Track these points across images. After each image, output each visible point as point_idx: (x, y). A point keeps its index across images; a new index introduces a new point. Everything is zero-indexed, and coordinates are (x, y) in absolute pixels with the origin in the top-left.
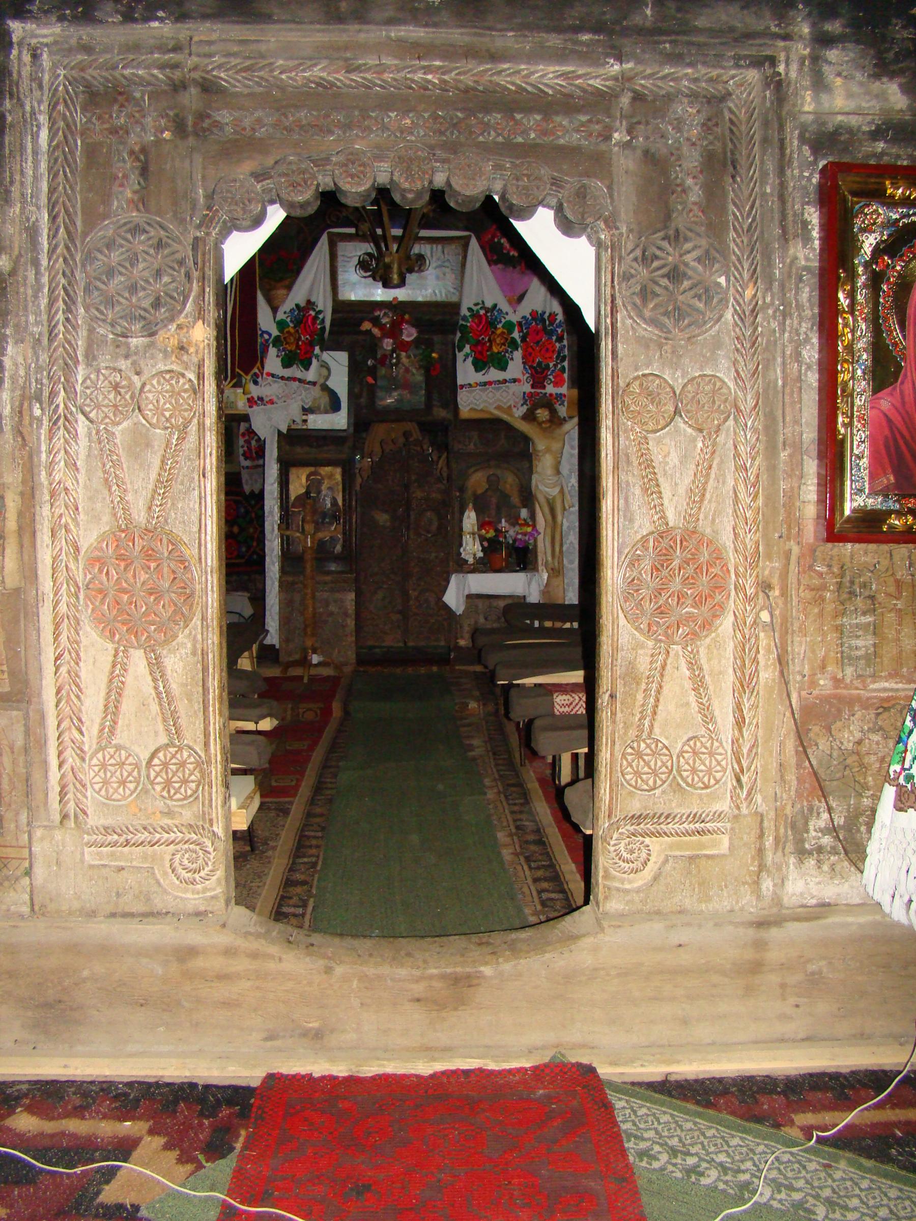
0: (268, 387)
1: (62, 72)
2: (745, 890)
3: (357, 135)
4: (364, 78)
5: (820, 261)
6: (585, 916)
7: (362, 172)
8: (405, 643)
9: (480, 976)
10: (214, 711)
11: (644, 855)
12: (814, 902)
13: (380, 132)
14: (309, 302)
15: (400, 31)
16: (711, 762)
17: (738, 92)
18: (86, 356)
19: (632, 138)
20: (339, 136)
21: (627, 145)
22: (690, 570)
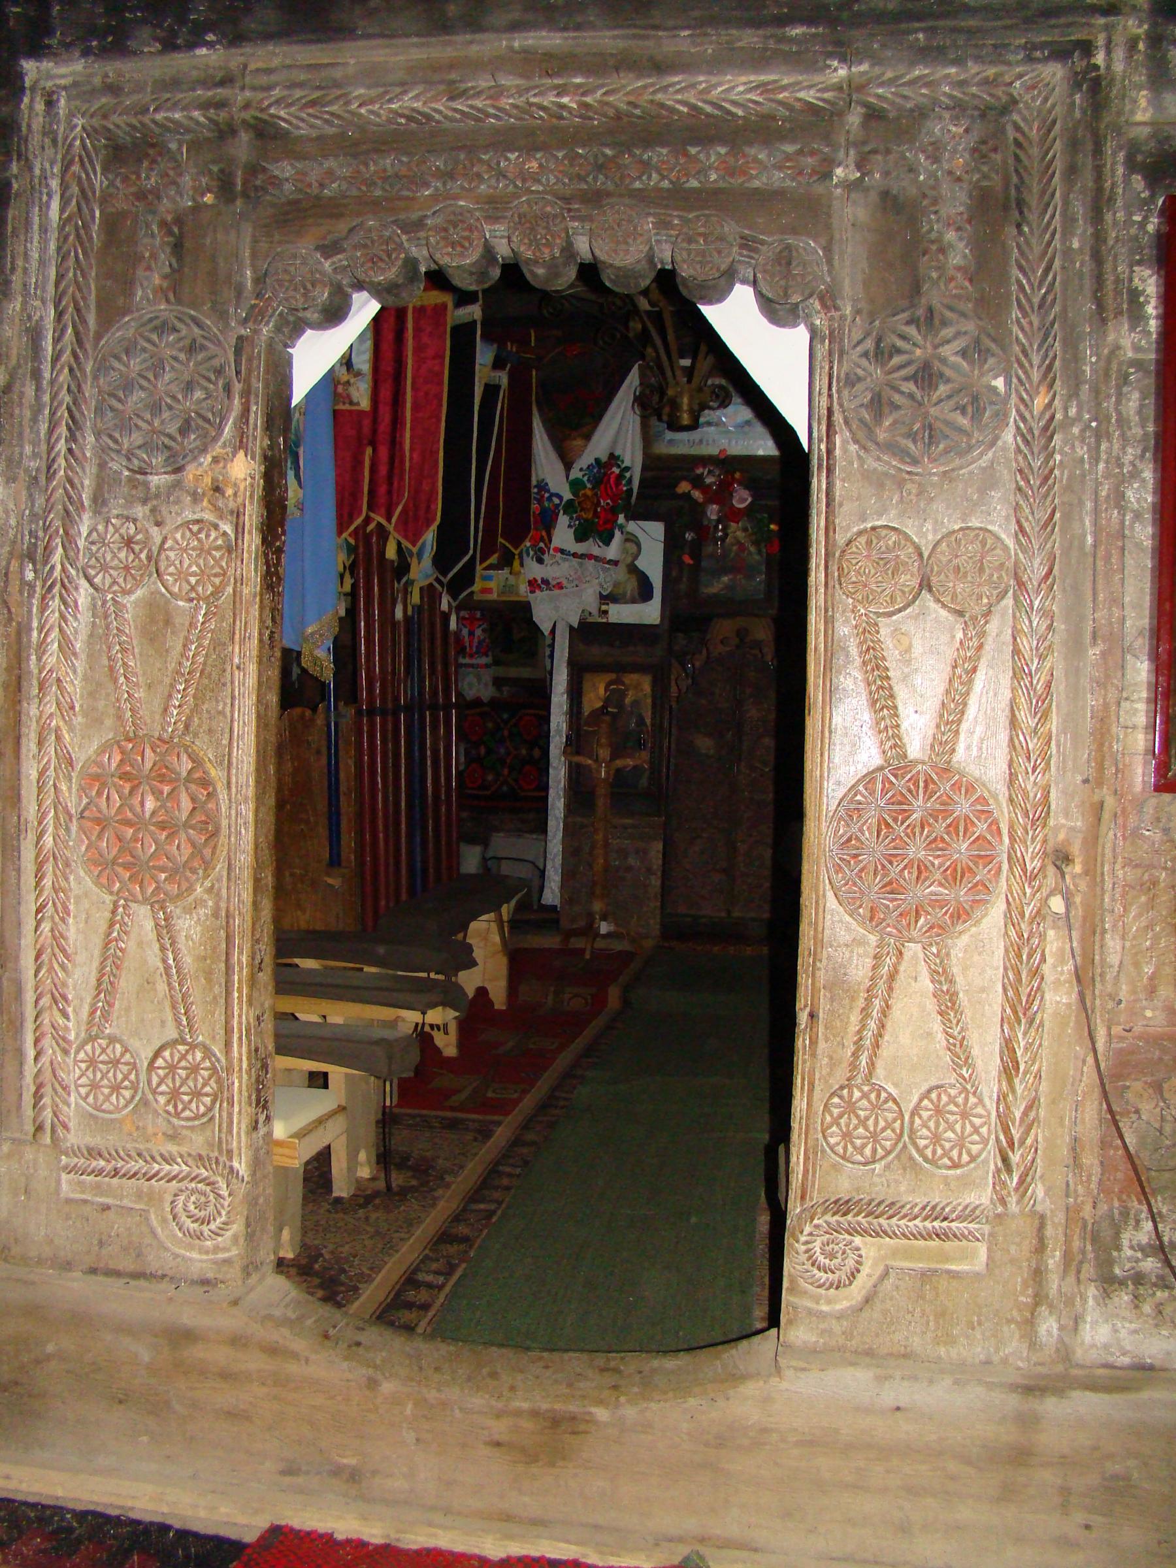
0: (555, 567)
1: (80, 122)
2: (1011, 1332)
3: (462, 188)
4: (471, 107)
5: (1157, 351)
6: (765, 1344)
7: (467, 239)
8: (729, 912)
9: (590, 1420)
10: (240, 998)
11: (850, 1263)
12: (1126, 1360)
13: (493, 182)
14: (612, 456)
15: (526, 39)
16: (963, 1128)
17: (1027, 97)
18: (95, 500)
19: (863, 175)
20: (437, 189)
21: (850, 186)
22: (940, 827)
